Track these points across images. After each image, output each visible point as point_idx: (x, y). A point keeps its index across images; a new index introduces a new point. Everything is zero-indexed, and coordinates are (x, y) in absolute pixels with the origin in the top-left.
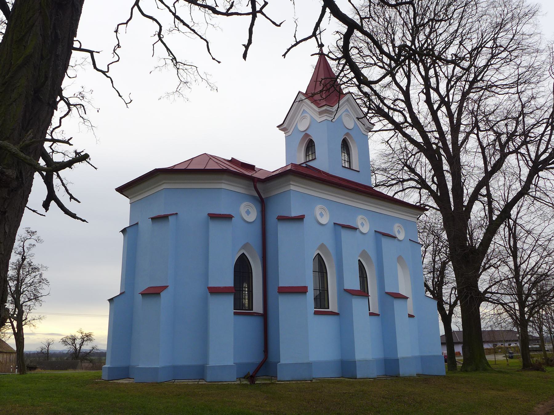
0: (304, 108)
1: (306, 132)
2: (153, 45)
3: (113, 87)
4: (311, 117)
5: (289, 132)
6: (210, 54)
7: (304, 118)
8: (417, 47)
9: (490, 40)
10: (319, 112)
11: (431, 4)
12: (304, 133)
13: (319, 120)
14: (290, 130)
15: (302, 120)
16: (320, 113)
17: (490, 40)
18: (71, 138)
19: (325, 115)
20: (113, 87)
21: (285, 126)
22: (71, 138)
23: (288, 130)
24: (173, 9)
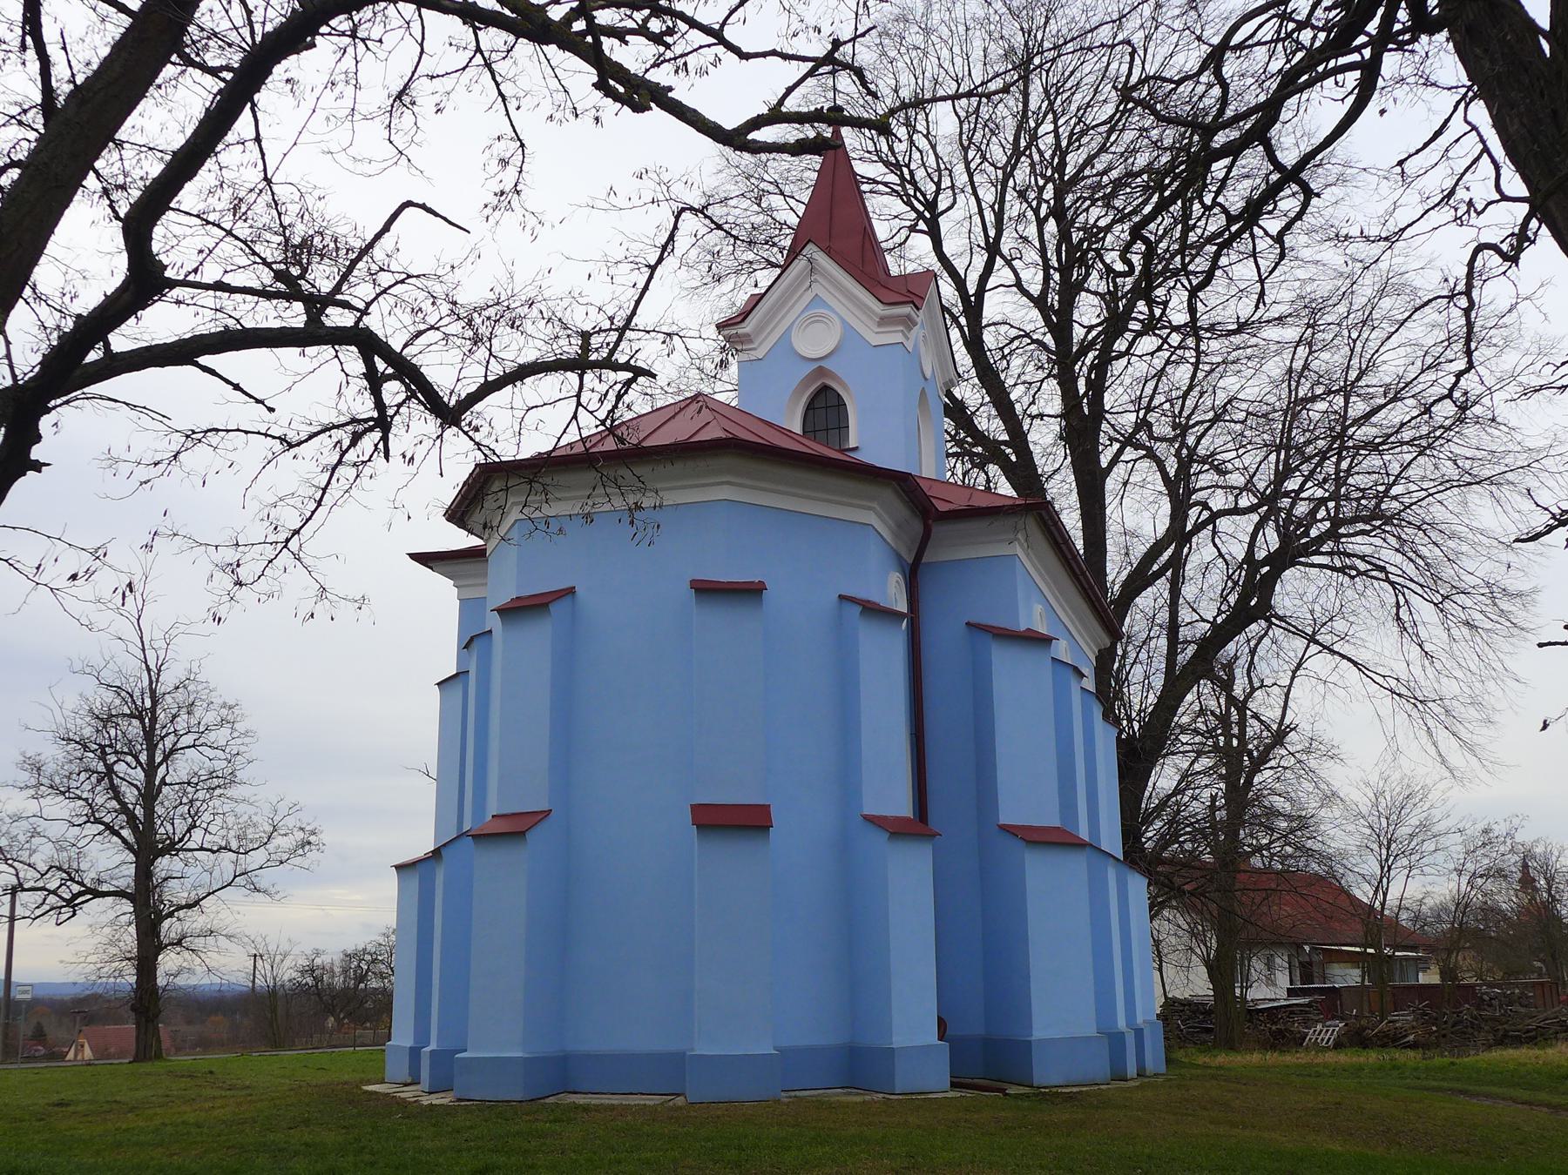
0: (816, 289)
1: (823, 364)
2: (409, 204)
3: (774, 53)
4: (843, 320)
5: (754, 349)
6: (436, 214)
7: (813, 322)
8: (846, 131)
9: (485, 455)
10: (882, 318)
11: (220, 46)
12: (815, 365)
13: (875, 340)
14: (760, 344)
15: (810, 323)
16: (884, 321)
17: (485, 455)
18: (49, 465)
19: (902, 328)
20: (774, 53)
21: (747, 327)
22: (49, 465)
23: (751, 341)
24: (416, 76)
